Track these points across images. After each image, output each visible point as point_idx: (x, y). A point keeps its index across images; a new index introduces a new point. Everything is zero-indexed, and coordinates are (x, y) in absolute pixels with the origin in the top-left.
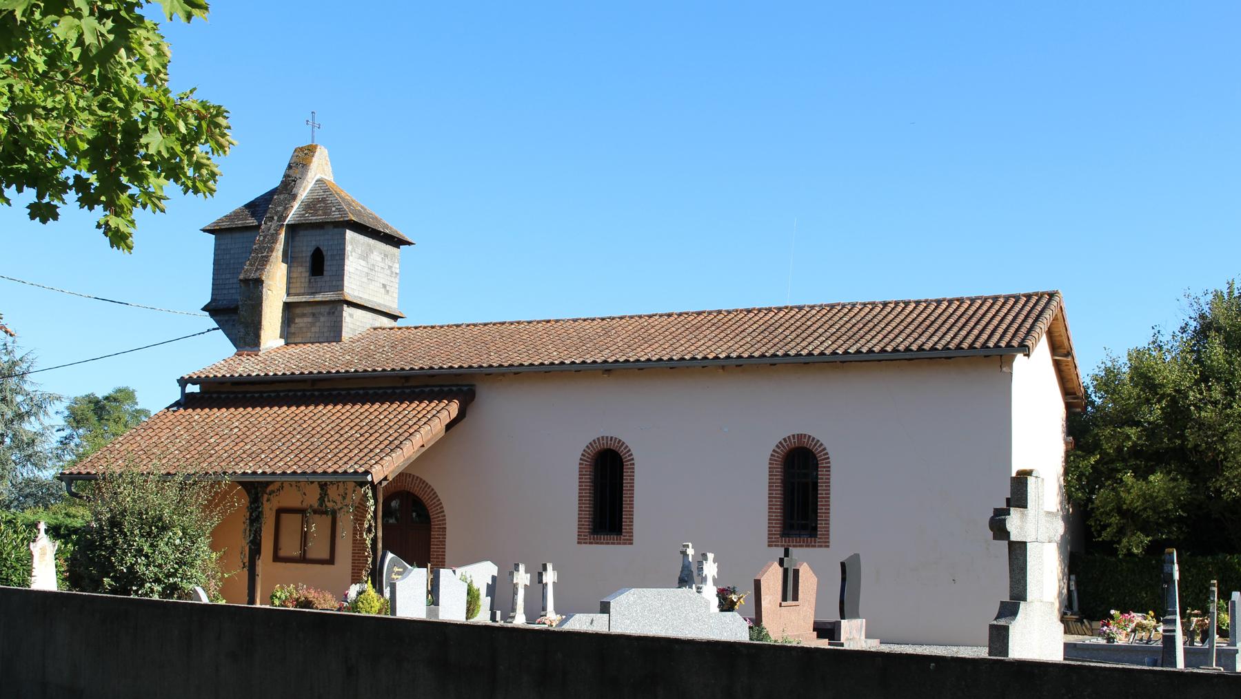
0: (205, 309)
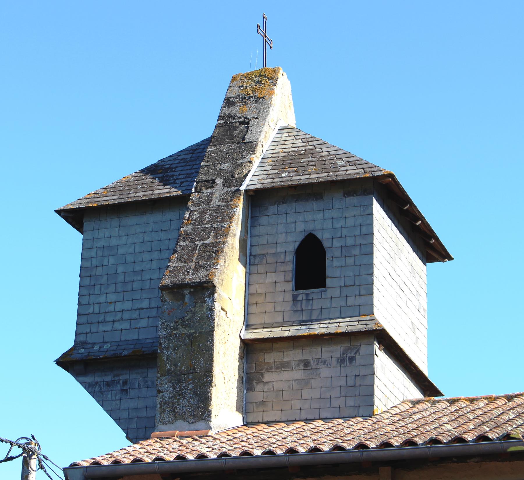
0: (66, 362)
